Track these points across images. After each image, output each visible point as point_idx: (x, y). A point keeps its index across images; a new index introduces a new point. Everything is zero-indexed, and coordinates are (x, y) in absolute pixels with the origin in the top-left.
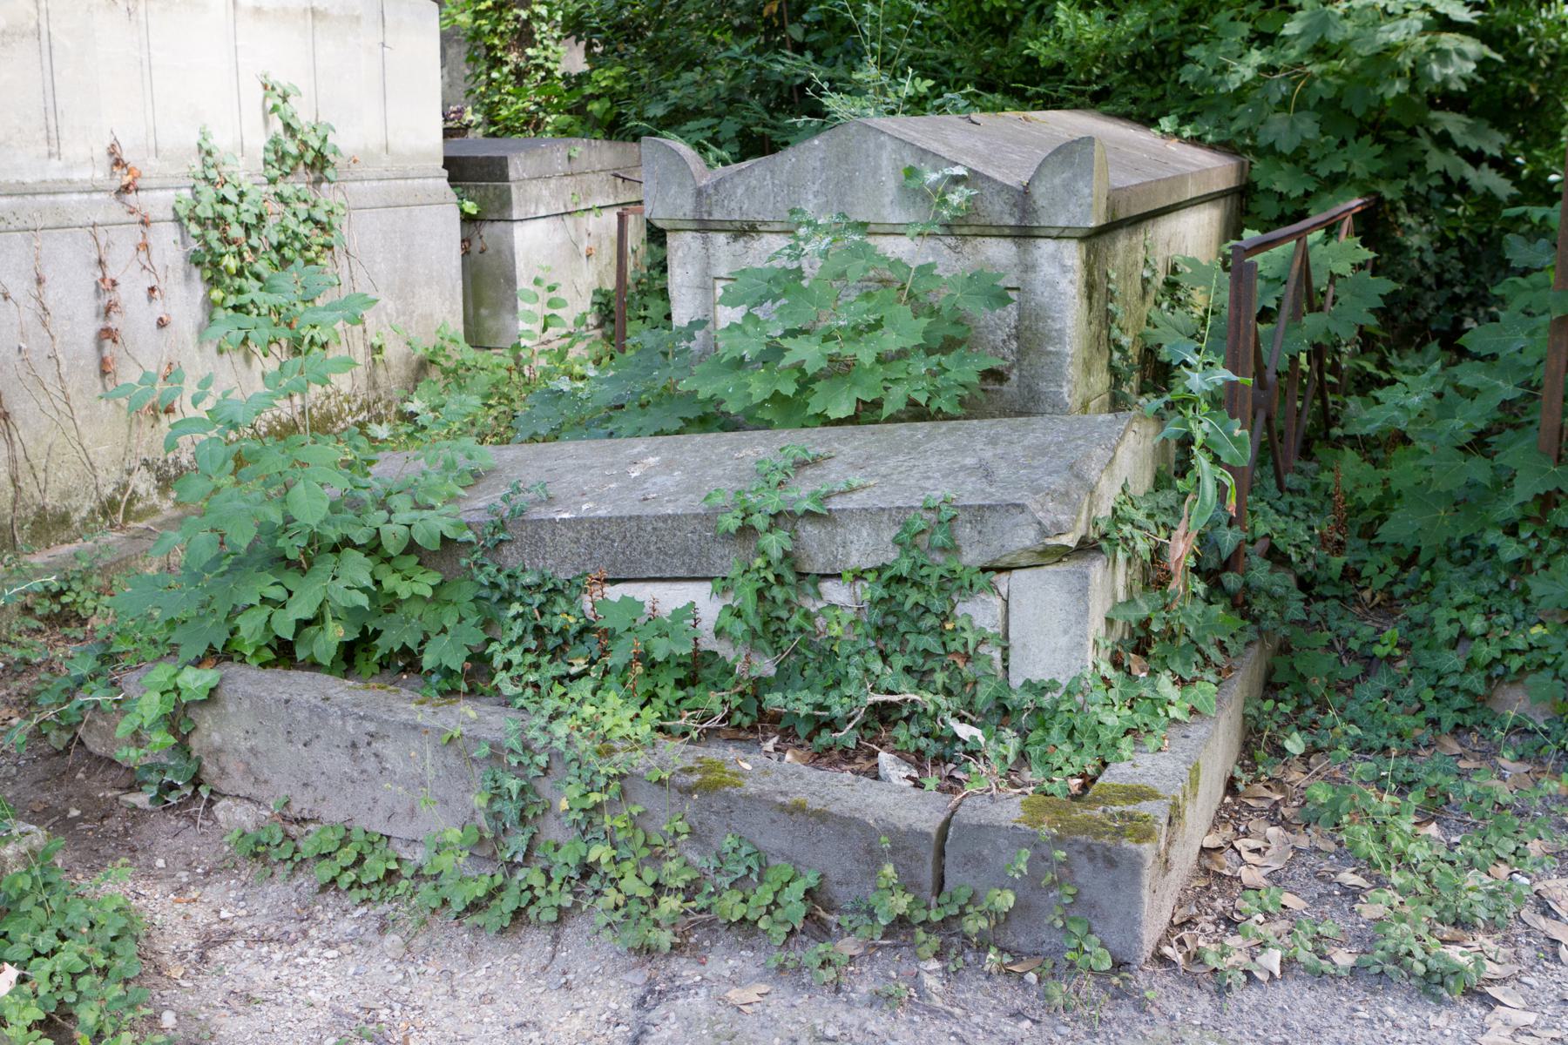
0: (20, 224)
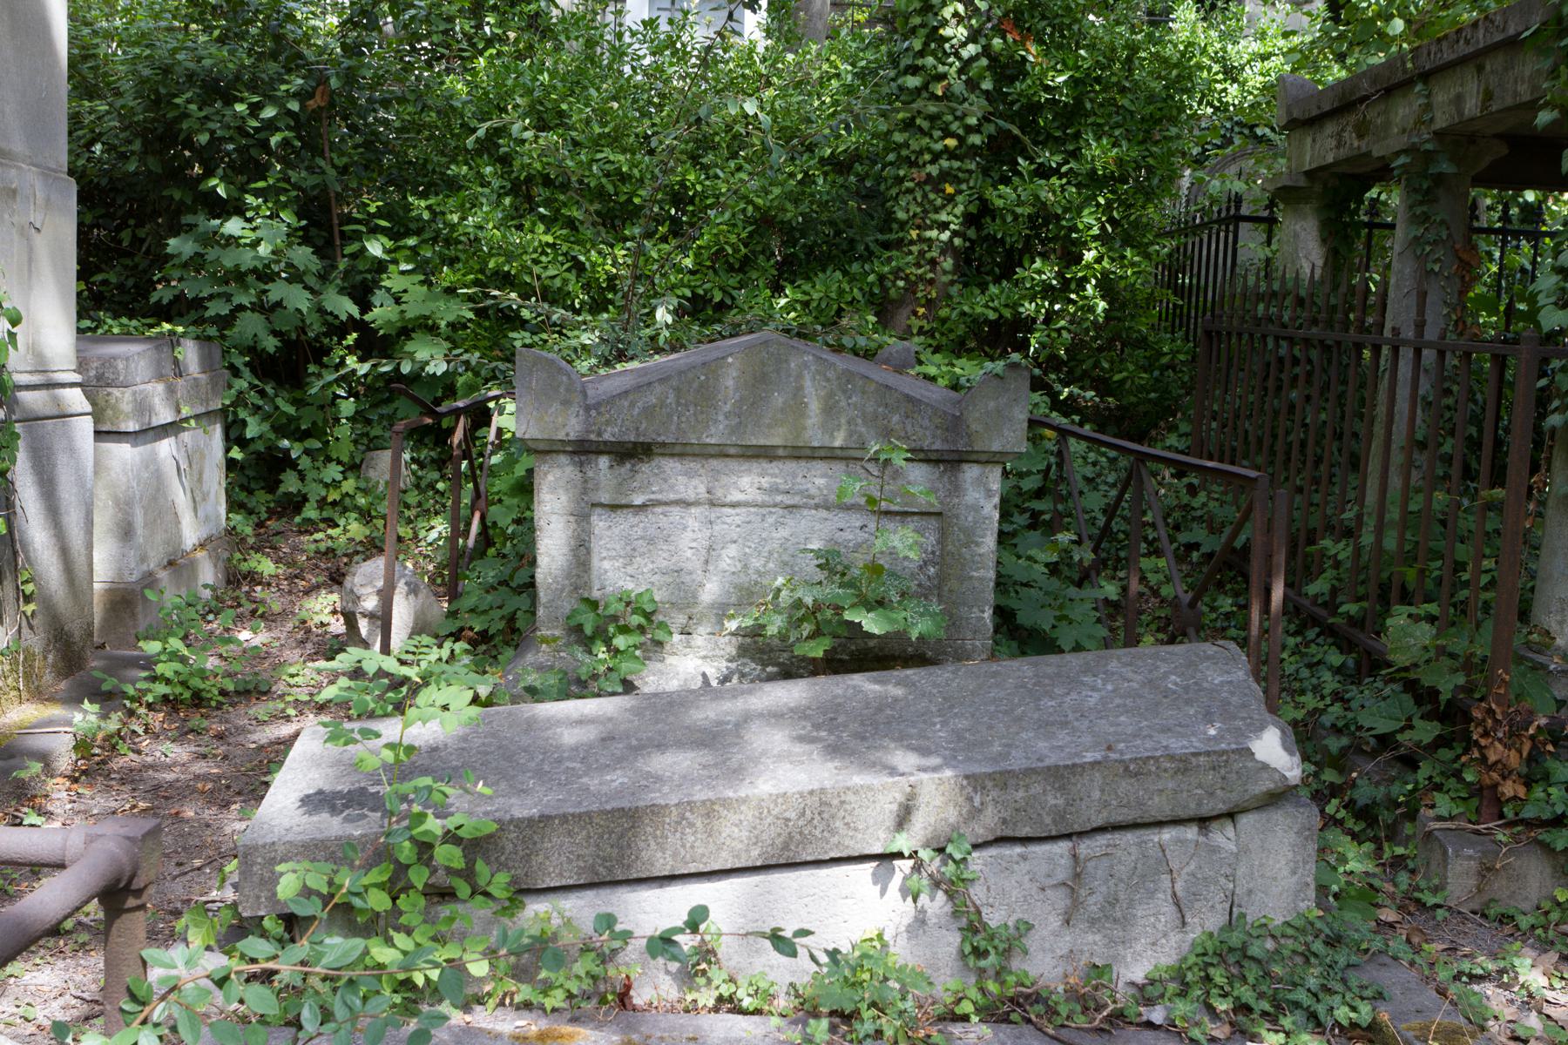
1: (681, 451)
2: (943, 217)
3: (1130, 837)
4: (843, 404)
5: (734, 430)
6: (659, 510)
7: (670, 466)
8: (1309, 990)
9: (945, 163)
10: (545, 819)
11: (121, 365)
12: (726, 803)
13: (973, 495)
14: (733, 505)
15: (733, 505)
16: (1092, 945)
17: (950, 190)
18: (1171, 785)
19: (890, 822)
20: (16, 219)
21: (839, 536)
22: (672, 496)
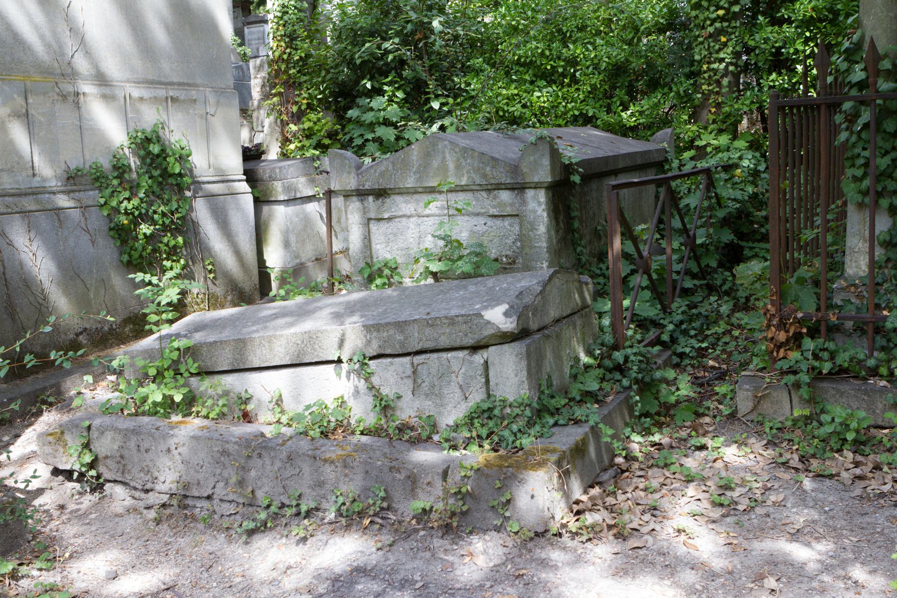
0: (17, 210)
1: (402, 192)
2: (722, 55)
3: (435, 355)
4: (464, 163)
5: (419, 179)
6: (397, 220)
7: (398, 199)
8: (512, 431)
9: (718, 25)
10: (215, 342)
11: (277, 171)
12: (275, 337)
13: (532, 205)
14: (428, 216)
15: (428, 216)
16: (428, 406)
17: (723, 39)
18: (447, 331)
19: (336, 346)
20: (197, 112)
21: (476, 229)
22: (401, 213)
